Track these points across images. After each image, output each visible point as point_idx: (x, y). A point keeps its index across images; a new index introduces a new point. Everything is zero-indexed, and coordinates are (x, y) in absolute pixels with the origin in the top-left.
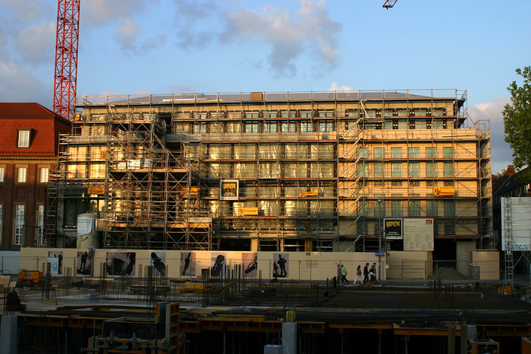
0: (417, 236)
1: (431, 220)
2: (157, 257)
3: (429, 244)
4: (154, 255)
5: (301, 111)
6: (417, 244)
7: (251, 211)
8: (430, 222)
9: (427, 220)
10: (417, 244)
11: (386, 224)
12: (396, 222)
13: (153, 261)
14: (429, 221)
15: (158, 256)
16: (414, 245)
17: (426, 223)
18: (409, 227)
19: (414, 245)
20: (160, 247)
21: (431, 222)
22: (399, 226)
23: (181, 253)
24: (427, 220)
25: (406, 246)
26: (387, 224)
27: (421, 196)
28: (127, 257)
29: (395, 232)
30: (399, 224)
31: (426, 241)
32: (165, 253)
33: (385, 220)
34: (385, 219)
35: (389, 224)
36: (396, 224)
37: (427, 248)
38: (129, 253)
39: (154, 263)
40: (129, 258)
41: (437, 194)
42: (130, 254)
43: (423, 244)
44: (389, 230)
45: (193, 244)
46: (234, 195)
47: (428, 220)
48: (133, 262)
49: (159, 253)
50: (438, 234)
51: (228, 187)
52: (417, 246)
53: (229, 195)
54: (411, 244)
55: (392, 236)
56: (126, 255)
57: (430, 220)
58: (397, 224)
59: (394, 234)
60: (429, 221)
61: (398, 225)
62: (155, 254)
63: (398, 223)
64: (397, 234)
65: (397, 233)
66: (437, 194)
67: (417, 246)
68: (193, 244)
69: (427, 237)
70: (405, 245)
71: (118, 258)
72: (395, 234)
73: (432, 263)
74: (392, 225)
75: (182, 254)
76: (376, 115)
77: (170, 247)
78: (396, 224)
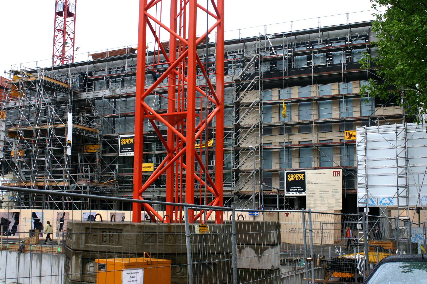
0: (322, 191)
1: (339, 171)
2: (37, 218)
3: (337, 201)
4: (34, 215)
5: (399, 116)
6: (322, 201)
7: (147, 167)
8: (338, 173)
9: (333, 172)
10: (322, 201)
11: (287, 177)
12: (299, 175)
13: (33, 221)
14: (336, 172)
15: (38, 216)
16: (319, 203)
17: (333, 175)
18: (312, 181)
19: (319, 203)
20: (39, 206)
21: (339, 173)
22: (303, 179)
23: (57, 213)
24: (333, 172)
25: (310, 204)
26: (289, 177)
27: (334, 141)
28: (13, 217)
29: (297, 187)
30: (303, 177)
31: (333, 197)
32: (123, 213)
33: (287, 173)
34: (286, 172)
35: (291, 178)
36: (299, 177)
37: (334, 206)
38: (14, 213)
39: (34, 223)
40: (14, 218)
41: (349, 138)
42: (15, 214)
43: (330, 201)
44: (291, 184)
45: (302, 209)
46: (132, 150)
47: (335, 171)
48: (17, 222)
49: (38, 212)
50: (354, 189)
51: (127, 143)
52: (322, 204)
53: (127, 151)
54: (315, 201)
55: (295, 193)
56: (12, 215)
57: (337, 171)
58: (301, 177)
59: (297, 189)
60: (336, 172)
61: (301, 178)
62: (35, 214)
63: (302, 177)
64: (301, 190)
65: (301, 189)
66: (349, 138)
67: (322, 204)
68: (302, 209)
69: (334, 192)
70: (307, 203)
71: (5, 218)
72: (298, 190)
73: (340, 225)
74: (295, 179)
75: (58, 214)
76: (308, 63)
77: (52, 207)
78: (299, 177)
